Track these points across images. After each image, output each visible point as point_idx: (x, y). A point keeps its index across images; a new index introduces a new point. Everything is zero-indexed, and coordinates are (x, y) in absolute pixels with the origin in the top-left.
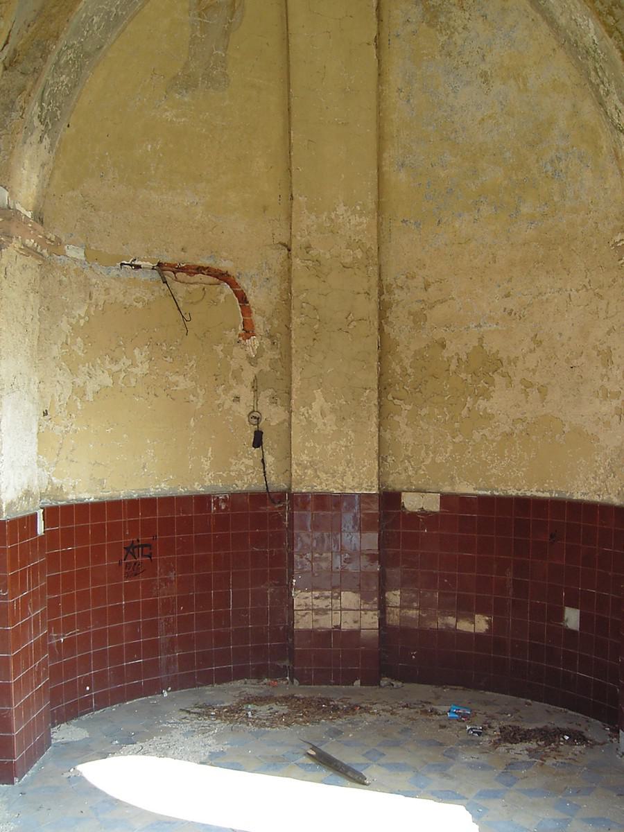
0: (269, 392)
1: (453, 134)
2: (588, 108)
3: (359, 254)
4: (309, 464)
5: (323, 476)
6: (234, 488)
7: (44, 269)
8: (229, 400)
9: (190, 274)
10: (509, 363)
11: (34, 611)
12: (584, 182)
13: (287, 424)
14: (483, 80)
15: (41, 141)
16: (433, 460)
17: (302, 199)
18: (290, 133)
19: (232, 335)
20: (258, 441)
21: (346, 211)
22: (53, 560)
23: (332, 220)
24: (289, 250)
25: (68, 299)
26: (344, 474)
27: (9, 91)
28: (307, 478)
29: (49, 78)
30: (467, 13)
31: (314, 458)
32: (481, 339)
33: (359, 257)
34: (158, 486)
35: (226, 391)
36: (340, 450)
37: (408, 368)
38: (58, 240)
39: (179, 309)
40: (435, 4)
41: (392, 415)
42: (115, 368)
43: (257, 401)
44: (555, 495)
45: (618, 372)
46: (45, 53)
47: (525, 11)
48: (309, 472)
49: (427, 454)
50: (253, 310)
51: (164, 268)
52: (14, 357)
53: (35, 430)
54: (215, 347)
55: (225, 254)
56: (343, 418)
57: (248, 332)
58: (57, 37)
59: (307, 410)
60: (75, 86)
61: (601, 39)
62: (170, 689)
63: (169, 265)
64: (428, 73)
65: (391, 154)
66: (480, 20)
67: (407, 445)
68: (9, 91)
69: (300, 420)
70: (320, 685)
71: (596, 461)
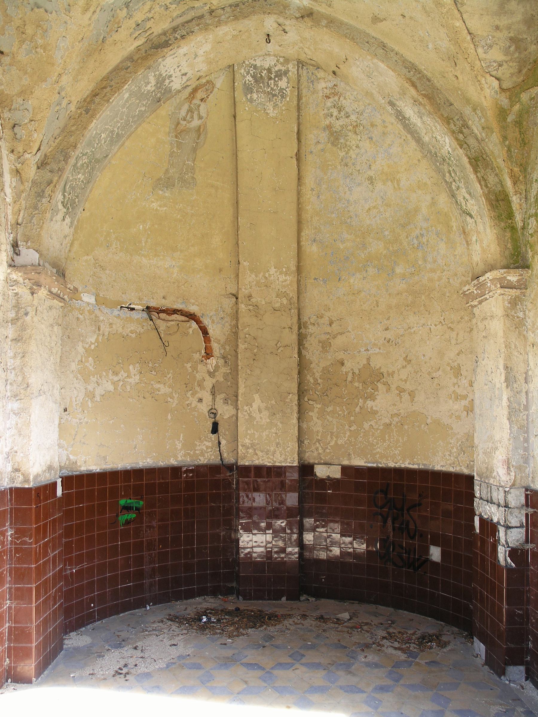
0: (223, 396)
1: (349, 219)
2: (443, 200)
3: (285, 301)
4: (250, 445)
5: (260, 454)
6: (198, 462)
7: (66, 310)
8: (195, 402)
9: (168, 314)
10: (388, 374)
11: (53, 552)
12: (439, 251)
13: (234, 418)
14: (369, 182)
15: (64, 220)
16: (336, 442)
17: (246, 264)
18: (238, 218)
19: (197, 356)
20: (215, 429)
21: (276, 272)
22: (68, 514)
23: (266, 278)
24: (237, 298)
25: (83, 331)
26: (274, 453)
27: (40, 184)
28: (249, 455)
29: (70, 176)
30: (359, 137)
31: (254, 441)
32: (368, 359)
33: (285, 303)
34: (145, 461)
35: (193, 395)
36: (271, 436)
37: (318, 379)
38: (76, 289)
39: (161, 338)
40: (337, 130)
41: (307, 411)
42: (116, 379)
43: (215, 401)
44: (421, 467)
45: (466, 381)
46: (66, 158)
47: (399, 134)
48: (250, 451)
49: (332, 438)
50: (212, 339)
51: (151, 310)
52: (41, 370)
53: (57, 422)
54: (185, 364)
55: (193, 301)
56: (274, 414)
57: (208, 354)
58: (75, 147)
59: (249, 408)
60: (88, 182)
61: (454, 150)
62: (151, 604)
63: (154, 308)
64: (332, 178)
65: (306, 233)
66: (368, 141)
67: (318, 432)
68: (40, 184)
69: (244, 415)
70: (258, 600)
71: (451, 443)
